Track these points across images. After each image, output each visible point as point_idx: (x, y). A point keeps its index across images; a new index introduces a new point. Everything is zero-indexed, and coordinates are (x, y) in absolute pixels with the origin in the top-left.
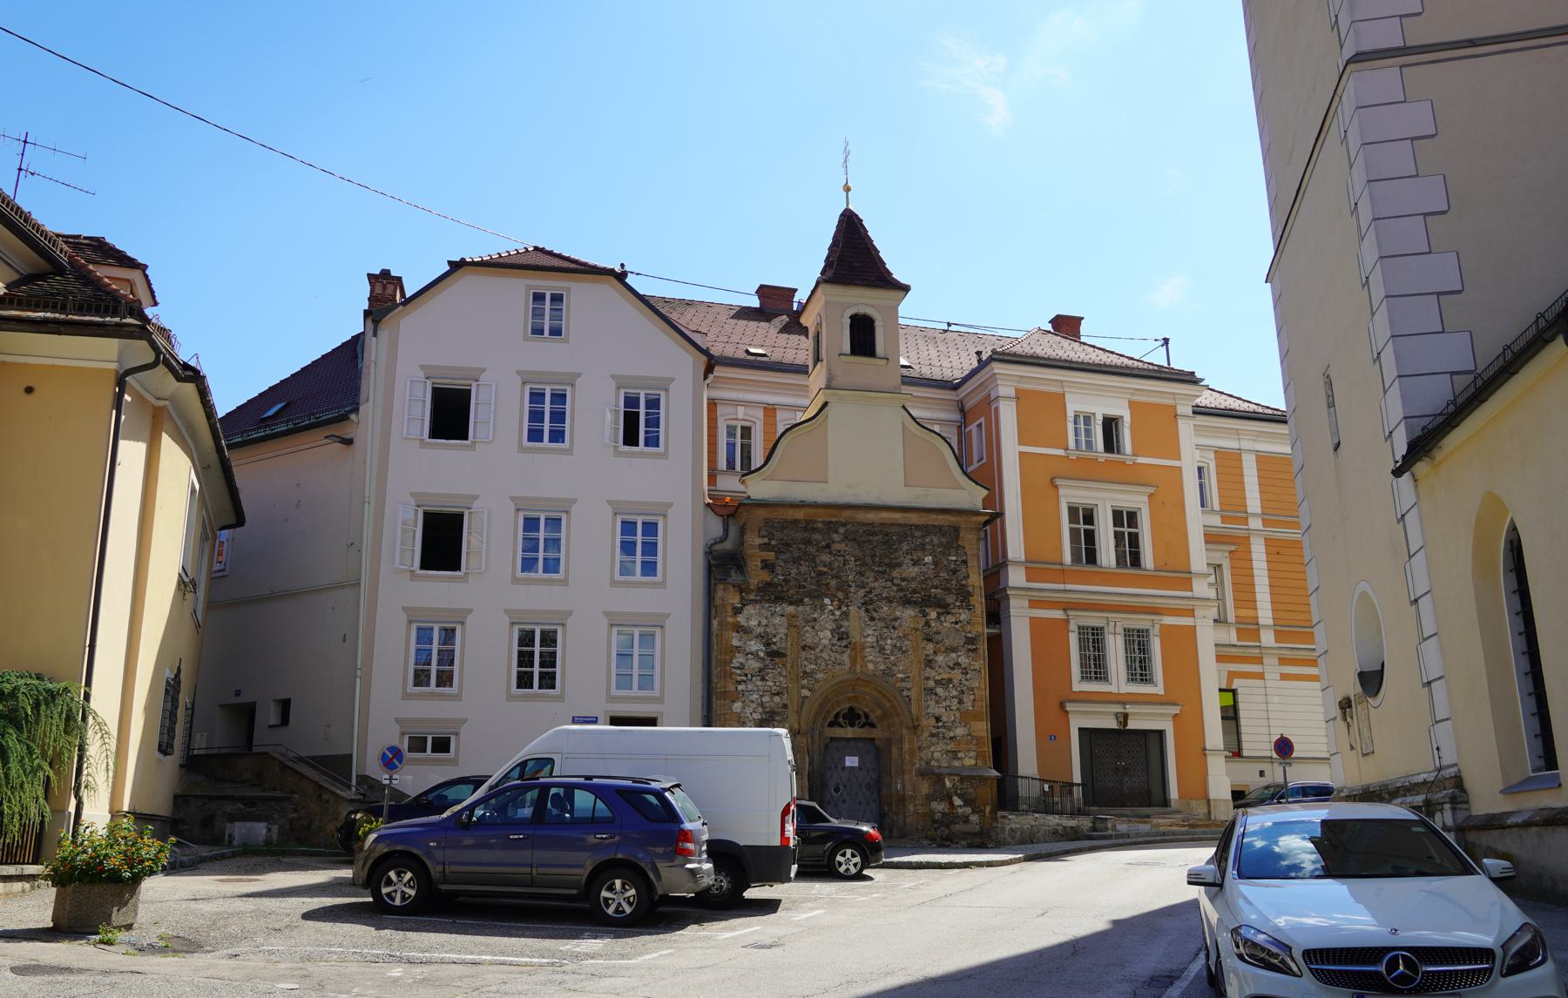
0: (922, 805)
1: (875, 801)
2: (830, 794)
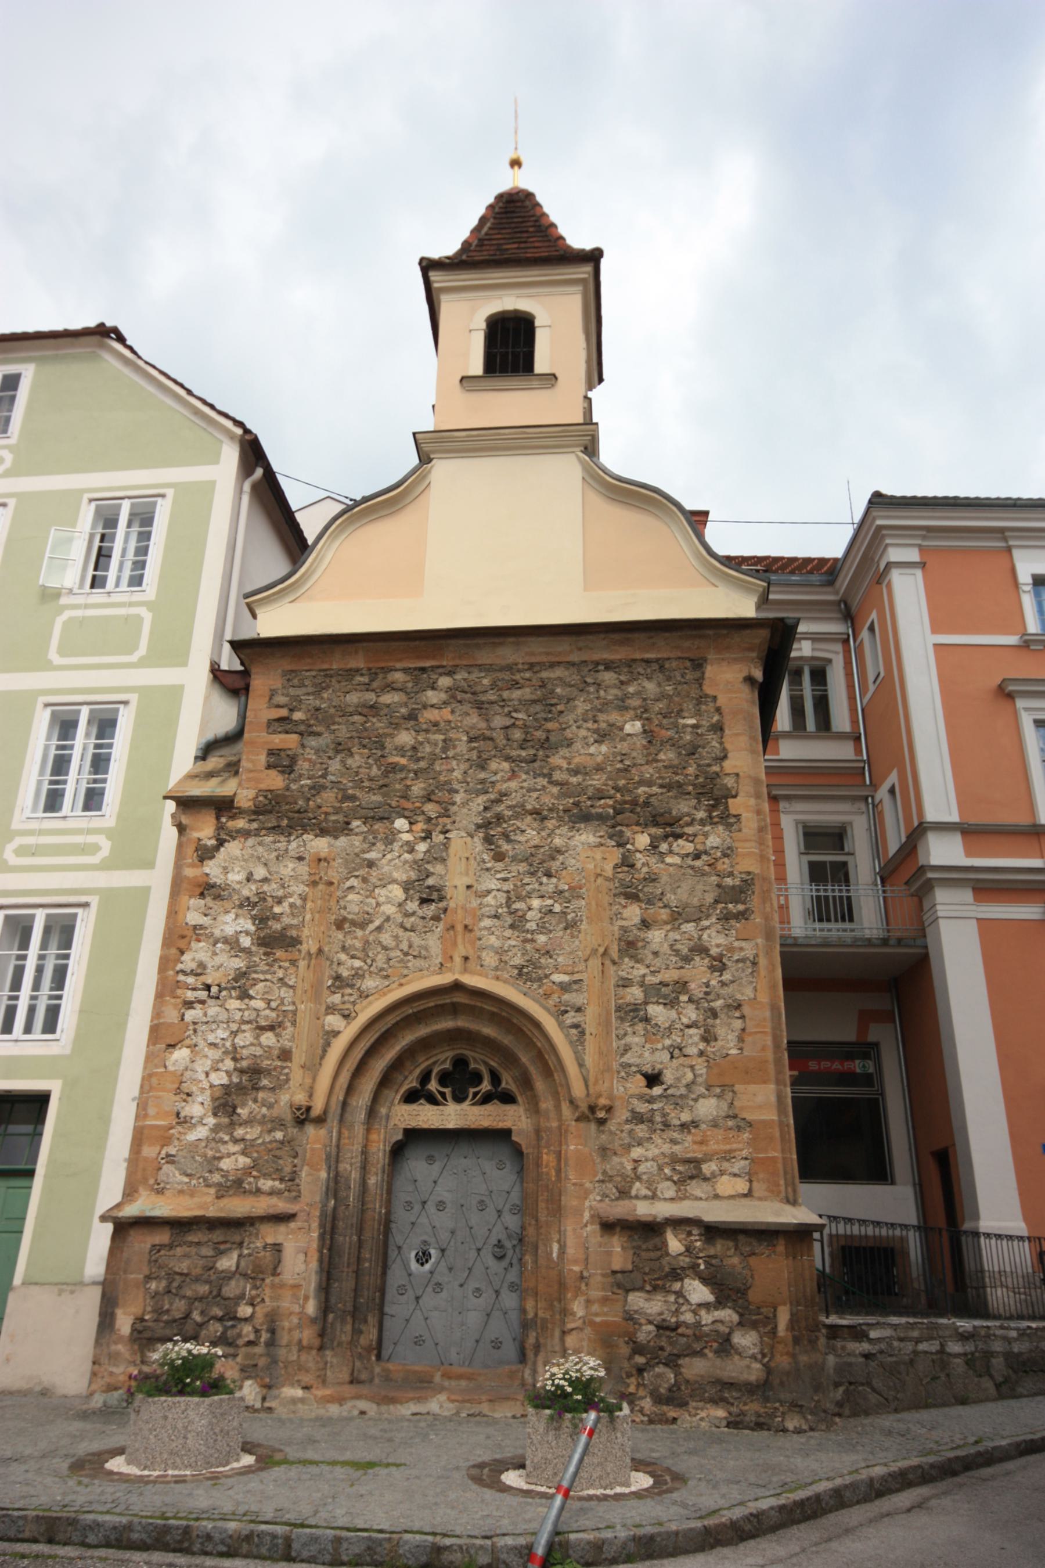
2: (406, 1266)
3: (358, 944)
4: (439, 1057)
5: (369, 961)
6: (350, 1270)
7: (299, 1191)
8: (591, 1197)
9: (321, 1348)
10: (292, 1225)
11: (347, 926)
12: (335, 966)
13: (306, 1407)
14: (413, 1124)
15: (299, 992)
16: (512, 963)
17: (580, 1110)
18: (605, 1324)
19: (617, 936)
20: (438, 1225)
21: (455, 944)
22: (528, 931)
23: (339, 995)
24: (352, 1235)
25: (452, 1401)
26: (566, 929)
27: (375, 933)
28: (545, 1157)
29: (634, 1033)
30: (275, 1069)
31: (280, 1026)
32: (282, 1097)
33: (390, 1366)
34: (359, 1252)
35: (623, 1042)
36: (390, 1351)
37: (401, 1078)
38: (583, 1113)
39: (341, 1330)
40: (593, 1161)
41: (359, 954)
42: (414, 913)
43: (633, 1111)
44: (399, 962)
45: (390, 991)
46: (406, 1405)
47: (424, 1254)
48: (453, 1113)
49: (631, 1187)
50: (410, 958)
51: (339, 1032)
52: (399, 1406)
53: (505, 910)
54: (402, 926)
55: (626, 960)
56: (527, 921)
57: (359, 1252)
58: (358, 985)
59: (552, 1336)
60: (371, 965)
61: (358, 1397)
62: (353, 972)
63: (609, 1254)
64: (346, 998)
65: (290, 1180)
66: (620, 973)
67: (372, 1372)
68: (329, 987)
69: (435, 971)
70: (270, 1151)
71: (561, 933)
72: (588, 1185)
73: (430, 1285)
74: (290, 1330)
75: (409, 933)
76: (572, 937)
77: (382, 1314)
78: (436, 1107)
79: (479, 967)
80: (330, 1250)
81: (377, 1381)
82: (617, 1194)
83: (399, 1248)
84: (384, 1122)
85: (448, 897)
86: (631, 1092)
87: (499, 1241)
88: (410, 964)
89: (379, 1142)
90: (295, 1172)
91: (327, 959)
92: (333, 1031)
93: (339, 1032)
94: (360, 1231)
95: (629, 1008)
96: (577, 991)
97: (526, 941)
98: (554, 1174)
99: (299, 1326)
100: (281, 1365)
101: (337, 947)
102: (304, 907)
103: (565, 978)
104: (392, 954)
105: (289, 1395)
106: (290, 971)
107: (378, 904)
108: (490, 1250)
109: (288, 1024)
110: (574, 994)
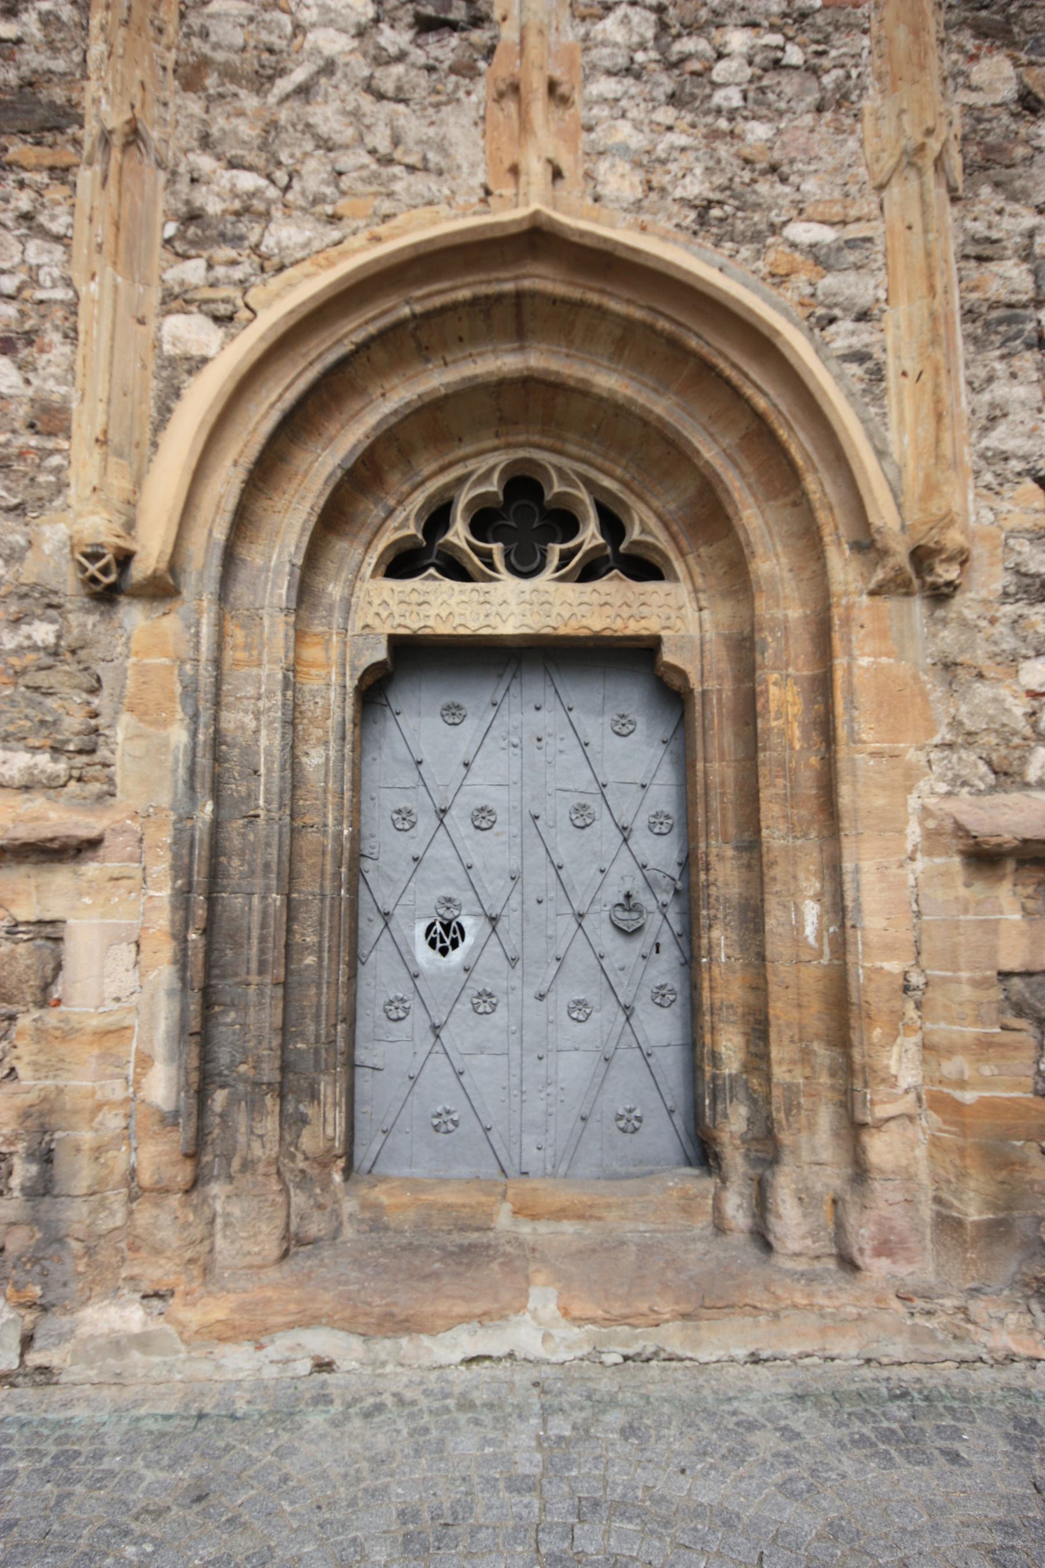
0: (984, 1046)
1: (660, 996)
2: (404, 957)
3: (247, 130)
4: (471, 465)
5: (281, 177)
6: (268, 979)
7: (110, 780)
8: (923, 785)
9: (195, 1184)
10: (91, 869)
11: (211, 81)
12: (183, 185)
13: (156, 1359)
14: (412, 624)
15: (81, 249)
16: (679, 193)
17: (891, 562)
18: (989, 1106)
19: (958, 129)
20: (475, 860)
21: (525, 126)
22: (719, 111)
23: (200, 264)
24: (268, 889)
25: (579, 1321)
26: (820, 109)
27: (295, 104)
28: (773, 690)
29: (1013, 376)
30: (21, 455)
31: (30, 343)
32: (47, 530)
33: (380, 1195)
34: (289, 931)
35: (986, 397)
36: (376, 1147)
37: (378, 513)
38: (900, 570)
39: (251, 1131)
40: (924, 695)
41: (251, 158)
42: (401, 57)
43: (1017, 571)
44: (367, 181)
45: (344, 255)
46: (446, 1337)
47: (446, 927)
48: (513, 600)
49: (1024, 760)
50: (397, 170)
51: (205, 360)
52: (425, 1340)
53: (654, 55)
54: (370, 88)
55: (985, 191)
56: (715, 86)
57: (289, 931)
58: (253, 238)
59: (811, 1126)
60: (287, 188)
61: (309, 1321)
62: (237, 205)
63: (991, 928)
64: (220, 271)
65: (80, 752)
66: (969, 224)
67: (336, 1214)
68: (168, 242)
69: (469, 205)
70: (24, 672)
71: (808, 119)
72: (913, 756)
73: (464, 998)
74: (99, 1151)
75: (388, 106)
76: (839, 130)
77: (351, 1065)
78: (469, 586)
79: (589, 201)
80: (207, 931)
81: (349, 1232)
82: (991, 778)
83: (386, 915)
84: (337, 619)
85: (497, 15)
86: (1013, 522)
87: (628, 896)
88: (398, 187)
89: (327, 665)
90: (96, 731)
91: (160, 164)
92: (188, 359)
93: (205, 360)
94: (289, 879)
95: (995, 314)
96: (858, 267)
97: (715, 134)
98: (797, 733)
99: (126, 1134)
100: (76, 1246)
101: (187, 138)
102: (85, 28)
103: (827, 235)
104: (346, 161)
105: (103, 1328)
106: (50, 195)
107: (299, 29)
108: (605, 915)
109: (56, 337)
110: (851, 277)
